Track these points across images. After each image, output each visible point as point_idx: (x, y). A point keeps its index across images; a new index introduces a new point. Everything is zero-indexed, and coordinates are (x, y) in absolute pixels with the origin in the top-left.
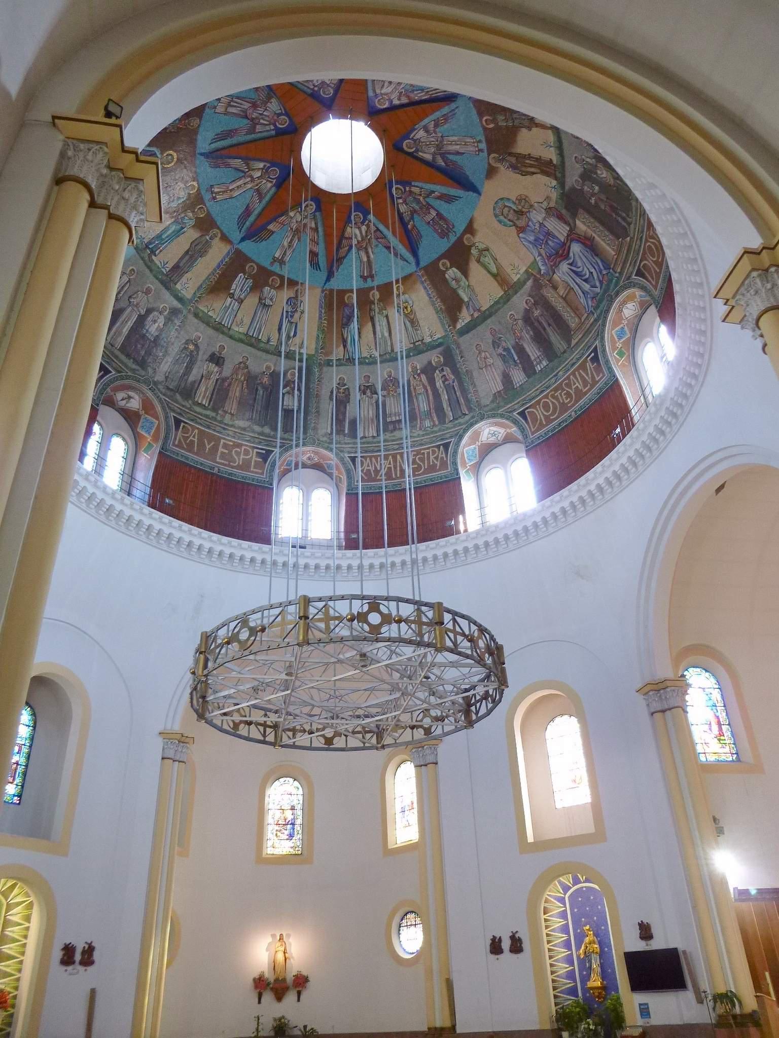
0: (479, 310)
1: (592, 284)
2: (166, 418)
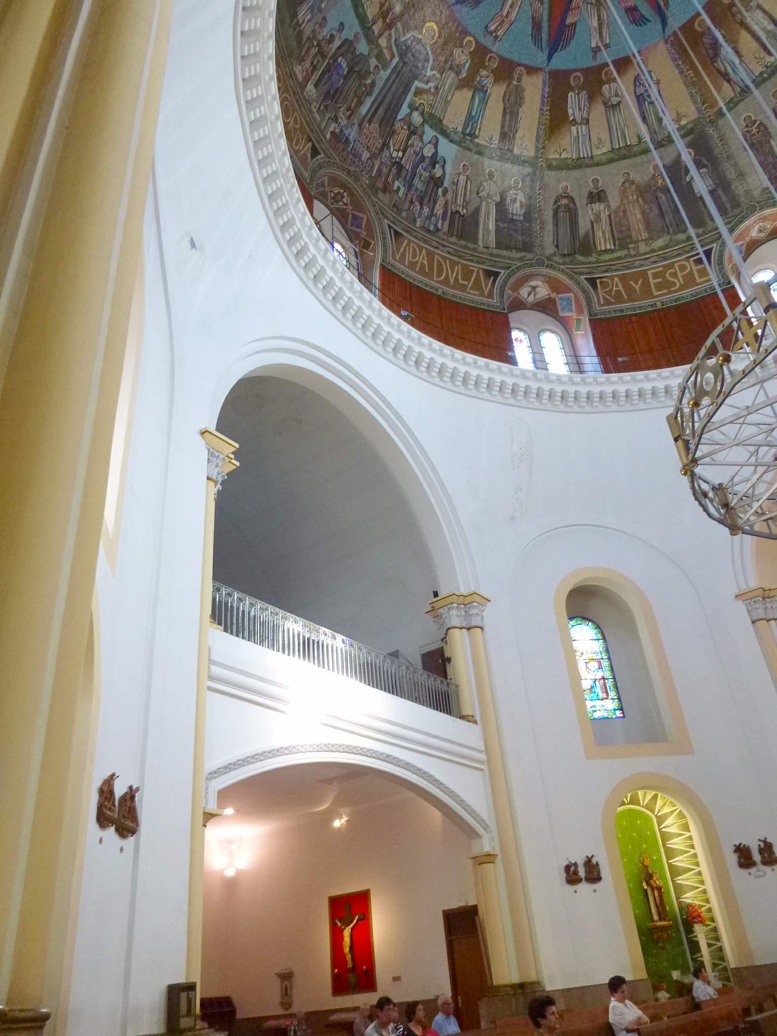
2: (578, 284)
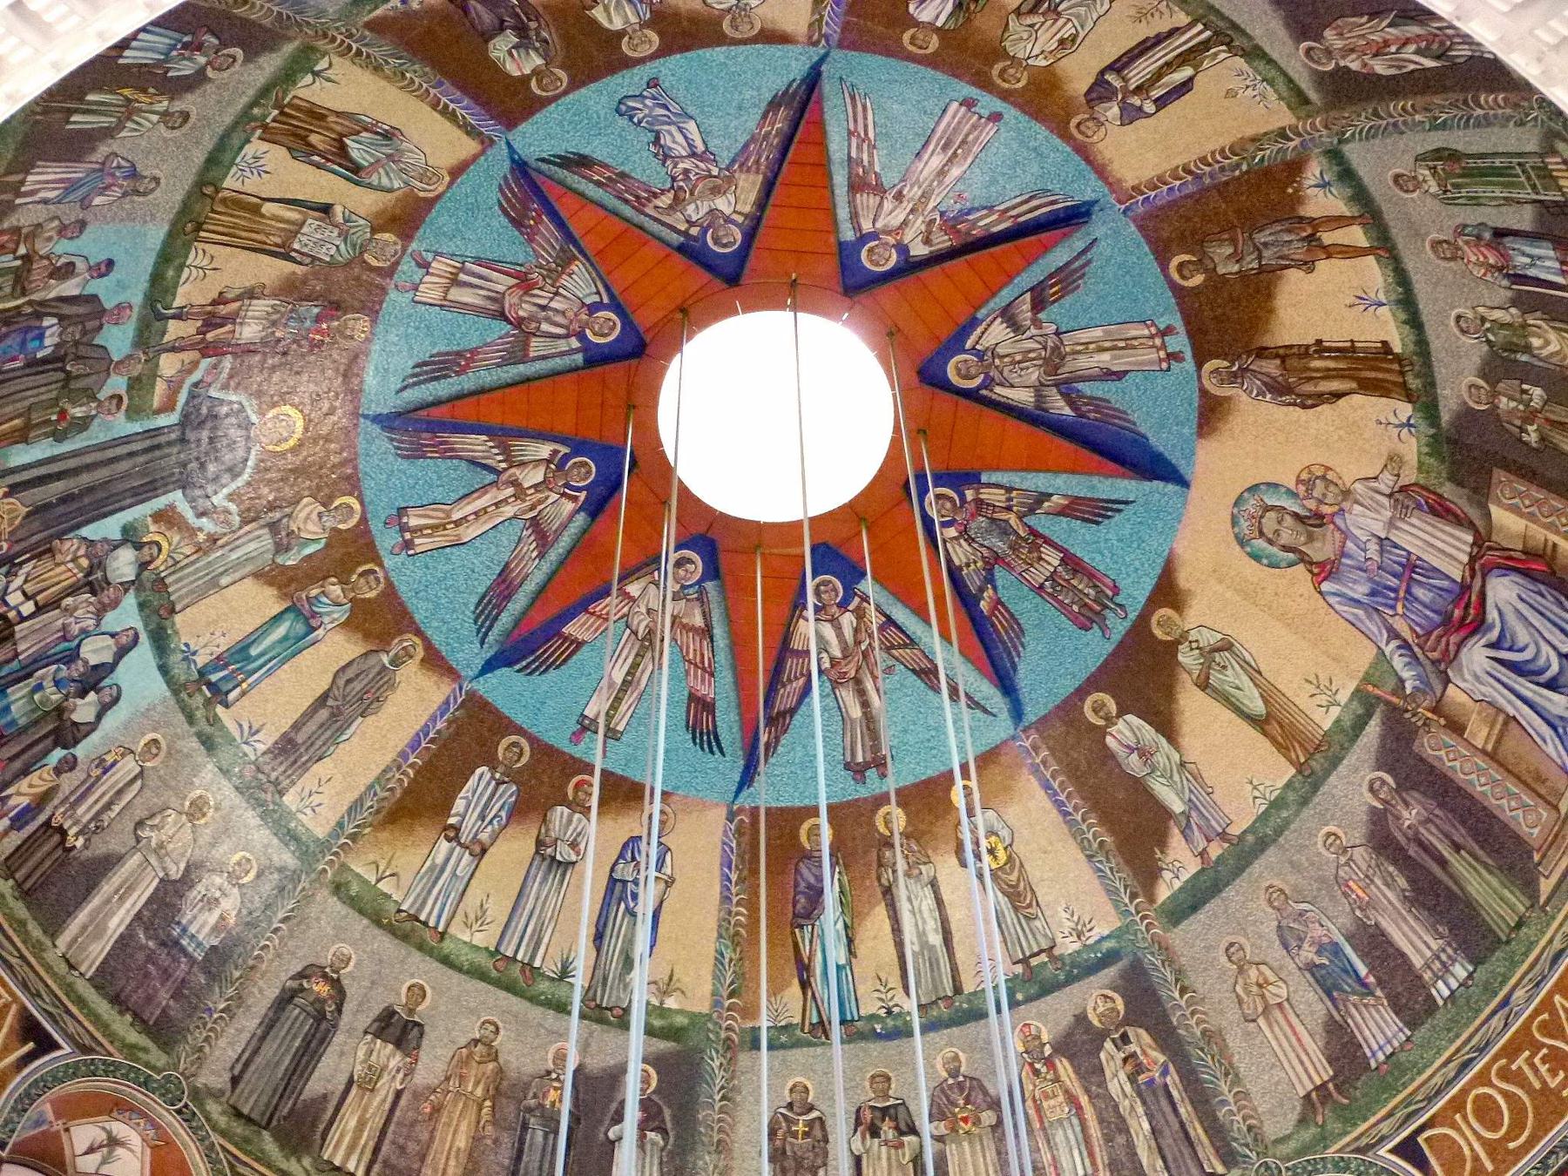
0: (1223, 836)
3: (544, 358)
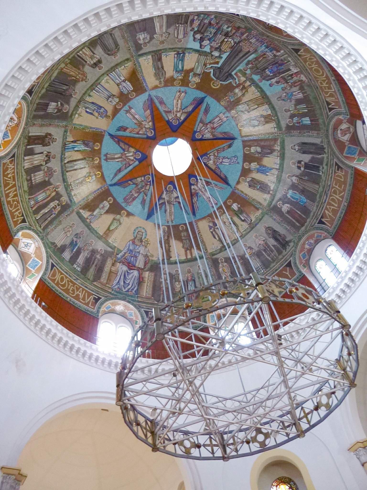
0: (91, 222)
1: (126, 286)
3: (198, 125)
